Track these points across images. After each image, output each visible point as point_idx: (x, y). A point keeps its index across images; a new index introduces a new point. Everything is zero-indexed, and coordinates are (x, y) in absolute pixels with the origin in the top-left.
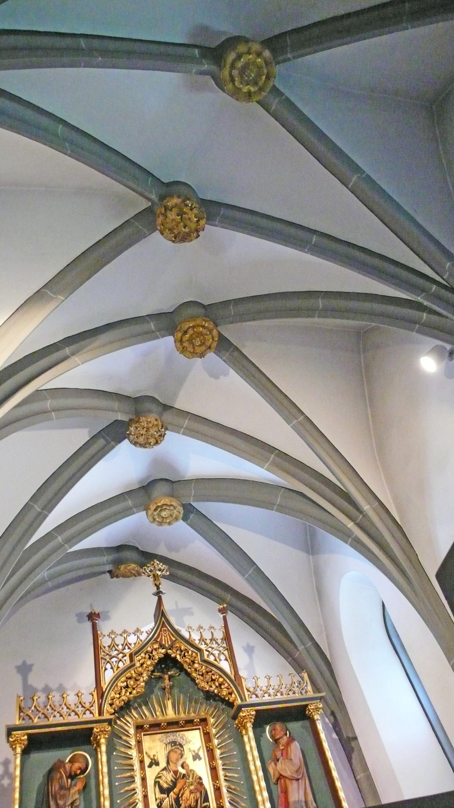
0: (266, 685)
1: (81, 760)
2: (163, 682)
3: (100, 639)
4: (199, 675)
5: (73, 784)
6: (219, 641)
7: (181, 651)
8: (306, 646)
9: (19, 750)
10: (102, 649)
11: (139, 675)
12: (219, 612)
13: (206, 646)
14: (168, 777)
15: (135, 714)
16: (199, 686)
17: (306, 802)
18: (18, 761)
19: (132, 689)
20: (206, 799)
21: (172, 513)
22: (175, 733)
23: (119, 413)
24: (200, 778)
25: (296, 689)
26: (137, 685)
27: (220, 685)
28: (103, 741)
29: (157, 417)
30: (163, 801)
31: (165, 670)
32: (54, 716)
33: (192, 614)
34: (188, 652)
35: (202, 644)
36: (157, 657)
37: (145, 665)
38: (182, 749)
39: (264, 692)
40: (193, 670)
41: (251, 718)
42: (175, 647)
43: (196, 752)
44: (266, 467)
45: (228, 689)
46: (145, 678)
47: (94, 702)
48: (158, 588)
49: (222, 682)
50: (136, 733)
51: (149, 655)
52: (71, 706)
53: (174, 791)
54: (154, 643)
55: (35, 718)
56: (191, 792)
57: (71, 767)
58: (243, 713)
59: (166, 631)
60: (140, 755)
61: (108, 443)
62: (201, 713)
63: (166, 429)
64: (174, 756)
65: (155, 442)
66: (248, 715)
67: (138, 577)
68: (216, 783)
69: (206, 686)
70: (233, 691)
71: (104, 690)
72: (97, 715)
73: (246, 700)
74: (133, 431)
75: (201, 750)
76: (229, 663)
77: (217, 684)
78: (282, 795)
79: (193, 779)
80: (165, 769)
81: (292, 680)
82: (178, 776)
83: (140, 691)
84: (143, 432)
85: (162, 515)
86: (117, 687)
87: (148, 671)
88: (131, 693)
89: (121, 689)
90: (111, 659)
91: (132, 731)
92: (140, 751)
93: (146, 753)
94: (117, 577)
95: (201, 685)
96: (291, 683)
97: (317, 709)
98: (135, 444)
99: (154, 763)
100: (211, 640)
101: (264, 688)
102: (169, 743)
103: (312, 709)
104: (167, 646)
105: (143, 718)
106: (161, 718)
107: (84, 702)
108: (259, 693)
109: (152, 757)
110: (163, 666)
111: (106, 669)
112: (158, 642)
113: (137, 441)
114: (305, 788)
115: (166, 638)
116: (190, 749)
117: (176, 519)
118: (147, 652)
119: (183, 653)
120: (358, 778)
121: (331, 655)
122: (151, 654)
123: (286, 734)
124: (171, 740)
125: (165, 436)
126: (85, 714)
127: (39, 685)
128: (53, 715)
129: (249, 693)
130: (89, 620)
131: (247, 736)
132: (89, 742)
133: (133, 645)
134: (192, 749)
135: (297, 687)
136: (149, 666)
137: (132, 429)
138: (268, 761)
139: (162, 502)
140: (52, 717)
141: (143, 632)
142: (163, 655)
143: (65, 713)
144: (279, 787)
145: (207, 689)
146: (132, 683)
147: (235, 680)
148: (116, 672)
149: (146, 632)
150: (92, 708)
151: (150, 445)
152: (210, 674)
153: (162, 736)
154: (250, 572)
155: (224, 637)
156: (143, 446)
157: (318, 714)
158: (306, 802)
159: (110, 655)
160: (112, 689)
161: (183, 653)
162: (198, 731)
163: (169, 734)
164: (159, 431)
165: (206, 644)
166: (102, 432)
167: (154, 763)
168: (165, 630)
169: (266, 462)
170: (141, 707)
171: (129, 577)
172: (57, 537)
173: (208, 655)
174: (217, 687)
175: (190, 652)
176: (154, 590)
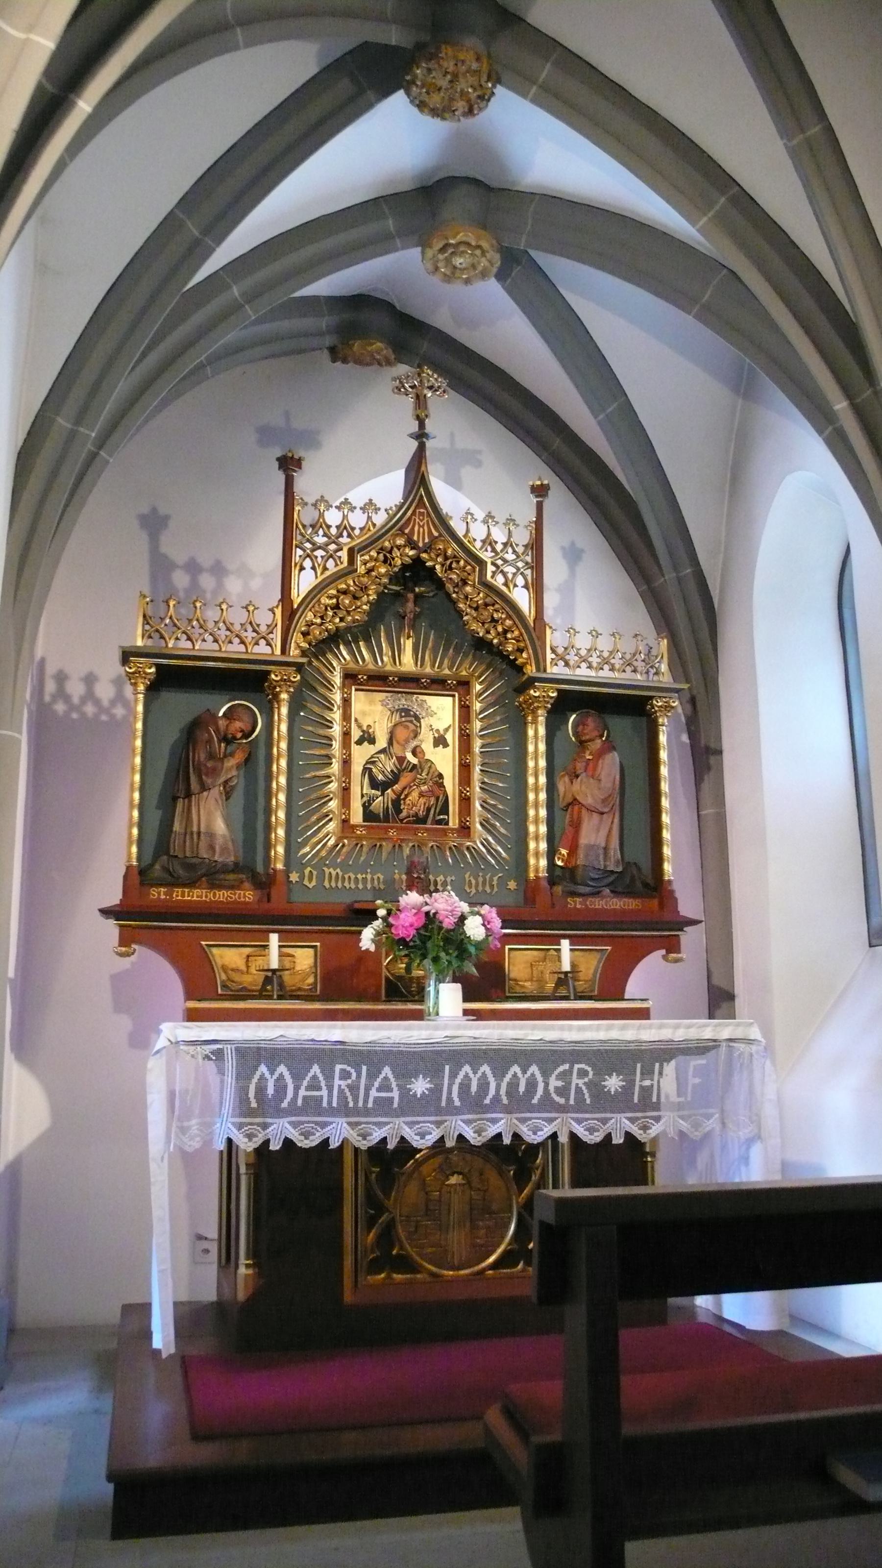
0: (588, 648)
1: (246, 718)
2: (403, 605)
3: (297, 508)
4: (470, 607)
5: (228, 751)
6: (520, 550)
7: (446, 558)
8: (681, 574)
9: (141, 688)
10: (300, 530)
11: (362, 589)
12: (532, 493)
13: (493, 554)
14: (389, 765)
15: (344, 653)
16: (467, 627)
17: (606, 849)
18: (140, 708)
19: (345, 612)
20: (445, 810)
21: (475, 261)
22: (409, 696)
23: (394, 27)
24: (441, 776)
25: (640, 665)
26: (357, 608)
27: (505, 632)
28: (284, 696)
29: (481, 48)
30: (374, 801)
31: (410, 585)
32: (204, 640)
33: (479, 464)
34: (458, 562)
35: (486, 550)
36: (399, 562)
37: (374, 574)
38: (418, 725)
39: (582, 659)
40: (462, 597)
41: (548, 702)
42: (435, 549)
43: (442, 732)
44: (701, 223)
45: (518, 641)
46: (371, 598)
47: (276, 625)
48: (422, 425)
49: (510, 627)
50: (344, 685)
51: (385, 556)
52: (235, 626)
53: (394, 787)
54: (397, 535)
55: (170, 639)
56: (421, 795)
57: (227, 726)
58: (535, 692)
59: (423, 516)
60: (345, 724)
61: (361, 92)
62: (462, 671)
63: (498, 81)
64: (401, 734)
65: (466, 110)
66: (544, 696)
67: (385, 368)
68: (465, 790)
69: (479, 630)
70: (526, 647)
71: (295, 606)
72: (278, 651)
73: (545, 670)
74: (420, 76)
75: (451, 730)
76: (530, 594)
77: (500, 629)
78: (569, 830)
79: (427, 775)
80: (383, 751)
81: (637, 647)
82: (403, 767)
83: (359, 618)
84: (444, 83)
85: (454, 263)
86: (319, 605)
87: (379, 584)
88: (342, 620)
89: (326, 609)
90: (313, 550)
91: (337, 679)
92: (346, 717)
93: (356, 720)
94: (345, 361)
95: (470, 627)
96: (633, 651)
97: (668, 708)
98: (421, 106)
99: (368, 738)
100: (505, 545)
101: (583, 653)
102: (397, 711)
103: (658, 707)
104: (421, 545)
105: (359, 663)
106: (389, 668)
107: (258, 623)
108: (572, 659)
109: (365, 728)
110: (407, 574)
111: (302, 568)
112: (406, 534)
113: (427, 100)
114: (610, 831)
115: (421, 530)
116: (431, 726)
117: (484, 275)
118: (382, 549)
119: (448, 562)
120: (702, 813)
121: (721, 600)
122: (388, 555)
123: (602, 736)
124: (401, 706)
125: (493, 99)
126: (258, 645)
127: (179, 556)
128: (202, 637)
129: (553, 656)
130: (280, 468)
131: (534, 725)
132: (261, 690)
133: (357, 532)
134: (435, 727)
135: (643, 661)
136: (382, 576)
137: (418, 72)
138: (559, 773)
139: (458, 237)
140: (199, 642)
141: (379, 509)
142: (412, 560)
143: (223, 638)
144: (568, 816)
145: (481, 634)
146: (347, 602)
147: (534, 629)
148: (320, 579)
149: (386, 510)
150: (271, 636)
151: (454, 115)
152: (491, 608)
153: (387, 697)
154: (610, 410)
155: (531, 542)
156: (435, 113)
157: (667, 716)
158: (606, 849)
159: (313, 544)
160: (308, 608)
161: (448, 562)
162: (451, 699)
163: (400, 695)
164: (481, 86)
165: (494, 550)
166: (347, 56)
167: (368, 738)
168: (422, 514)
169: (705, 214)
170: (357, 643)
171: (368, 364)
172: (229, 287)
173: (494, 573)
174: (498, 634)
175: (462, 563)
176: (414, 427)
